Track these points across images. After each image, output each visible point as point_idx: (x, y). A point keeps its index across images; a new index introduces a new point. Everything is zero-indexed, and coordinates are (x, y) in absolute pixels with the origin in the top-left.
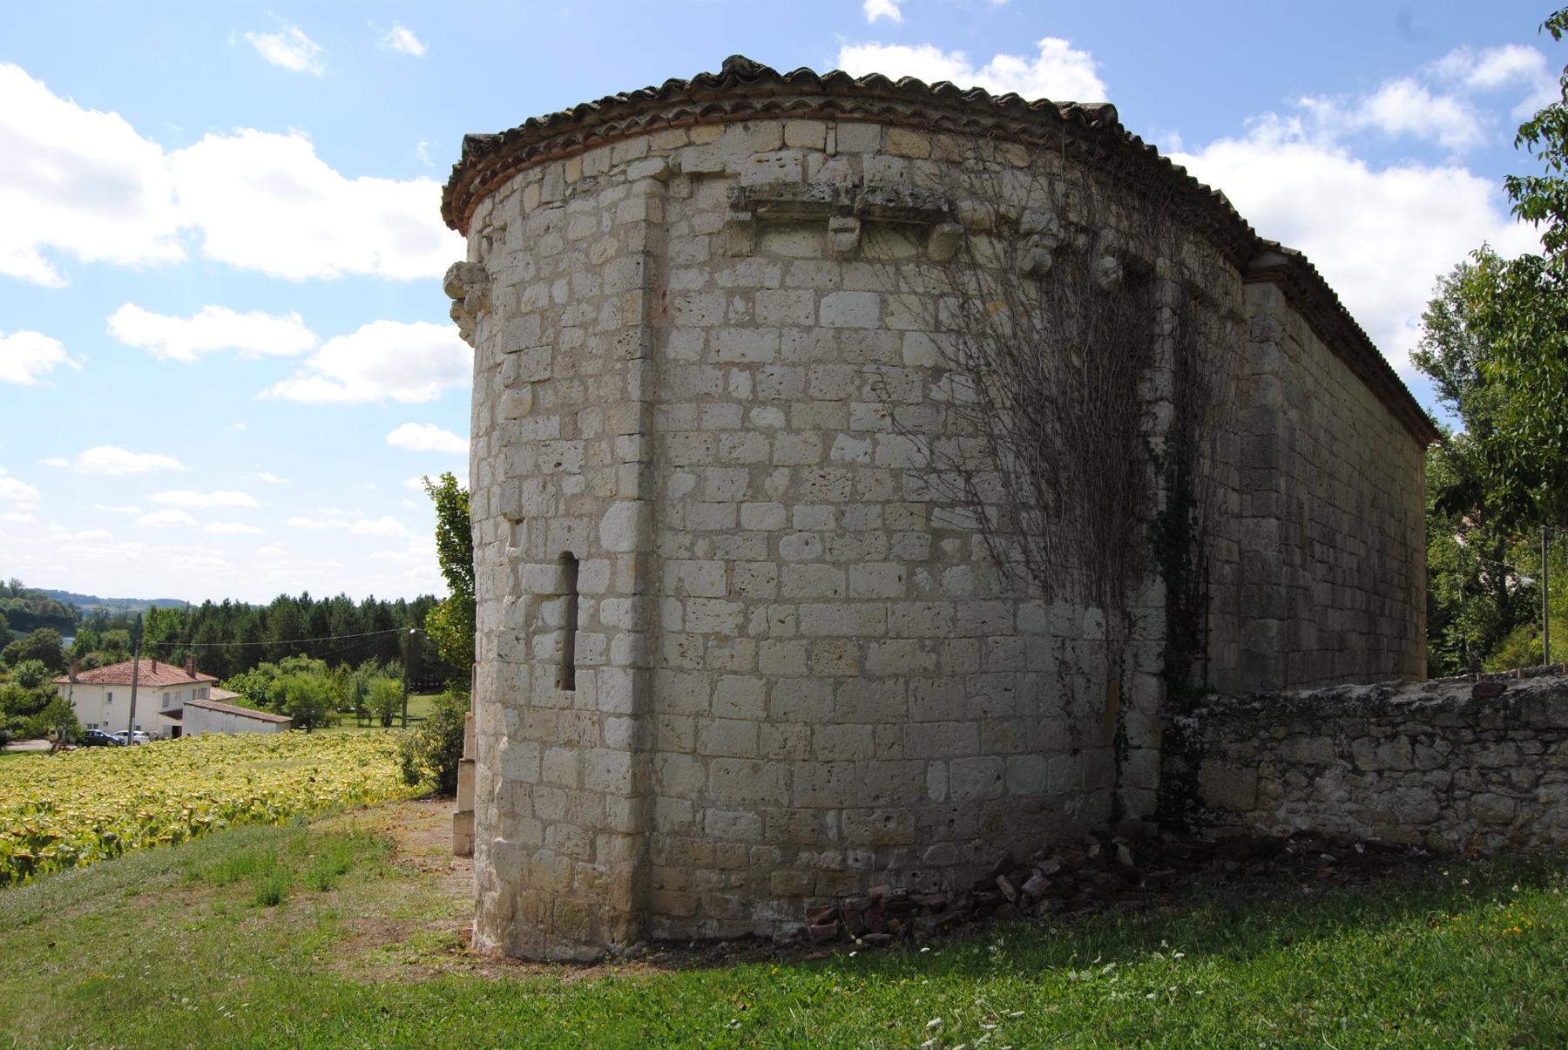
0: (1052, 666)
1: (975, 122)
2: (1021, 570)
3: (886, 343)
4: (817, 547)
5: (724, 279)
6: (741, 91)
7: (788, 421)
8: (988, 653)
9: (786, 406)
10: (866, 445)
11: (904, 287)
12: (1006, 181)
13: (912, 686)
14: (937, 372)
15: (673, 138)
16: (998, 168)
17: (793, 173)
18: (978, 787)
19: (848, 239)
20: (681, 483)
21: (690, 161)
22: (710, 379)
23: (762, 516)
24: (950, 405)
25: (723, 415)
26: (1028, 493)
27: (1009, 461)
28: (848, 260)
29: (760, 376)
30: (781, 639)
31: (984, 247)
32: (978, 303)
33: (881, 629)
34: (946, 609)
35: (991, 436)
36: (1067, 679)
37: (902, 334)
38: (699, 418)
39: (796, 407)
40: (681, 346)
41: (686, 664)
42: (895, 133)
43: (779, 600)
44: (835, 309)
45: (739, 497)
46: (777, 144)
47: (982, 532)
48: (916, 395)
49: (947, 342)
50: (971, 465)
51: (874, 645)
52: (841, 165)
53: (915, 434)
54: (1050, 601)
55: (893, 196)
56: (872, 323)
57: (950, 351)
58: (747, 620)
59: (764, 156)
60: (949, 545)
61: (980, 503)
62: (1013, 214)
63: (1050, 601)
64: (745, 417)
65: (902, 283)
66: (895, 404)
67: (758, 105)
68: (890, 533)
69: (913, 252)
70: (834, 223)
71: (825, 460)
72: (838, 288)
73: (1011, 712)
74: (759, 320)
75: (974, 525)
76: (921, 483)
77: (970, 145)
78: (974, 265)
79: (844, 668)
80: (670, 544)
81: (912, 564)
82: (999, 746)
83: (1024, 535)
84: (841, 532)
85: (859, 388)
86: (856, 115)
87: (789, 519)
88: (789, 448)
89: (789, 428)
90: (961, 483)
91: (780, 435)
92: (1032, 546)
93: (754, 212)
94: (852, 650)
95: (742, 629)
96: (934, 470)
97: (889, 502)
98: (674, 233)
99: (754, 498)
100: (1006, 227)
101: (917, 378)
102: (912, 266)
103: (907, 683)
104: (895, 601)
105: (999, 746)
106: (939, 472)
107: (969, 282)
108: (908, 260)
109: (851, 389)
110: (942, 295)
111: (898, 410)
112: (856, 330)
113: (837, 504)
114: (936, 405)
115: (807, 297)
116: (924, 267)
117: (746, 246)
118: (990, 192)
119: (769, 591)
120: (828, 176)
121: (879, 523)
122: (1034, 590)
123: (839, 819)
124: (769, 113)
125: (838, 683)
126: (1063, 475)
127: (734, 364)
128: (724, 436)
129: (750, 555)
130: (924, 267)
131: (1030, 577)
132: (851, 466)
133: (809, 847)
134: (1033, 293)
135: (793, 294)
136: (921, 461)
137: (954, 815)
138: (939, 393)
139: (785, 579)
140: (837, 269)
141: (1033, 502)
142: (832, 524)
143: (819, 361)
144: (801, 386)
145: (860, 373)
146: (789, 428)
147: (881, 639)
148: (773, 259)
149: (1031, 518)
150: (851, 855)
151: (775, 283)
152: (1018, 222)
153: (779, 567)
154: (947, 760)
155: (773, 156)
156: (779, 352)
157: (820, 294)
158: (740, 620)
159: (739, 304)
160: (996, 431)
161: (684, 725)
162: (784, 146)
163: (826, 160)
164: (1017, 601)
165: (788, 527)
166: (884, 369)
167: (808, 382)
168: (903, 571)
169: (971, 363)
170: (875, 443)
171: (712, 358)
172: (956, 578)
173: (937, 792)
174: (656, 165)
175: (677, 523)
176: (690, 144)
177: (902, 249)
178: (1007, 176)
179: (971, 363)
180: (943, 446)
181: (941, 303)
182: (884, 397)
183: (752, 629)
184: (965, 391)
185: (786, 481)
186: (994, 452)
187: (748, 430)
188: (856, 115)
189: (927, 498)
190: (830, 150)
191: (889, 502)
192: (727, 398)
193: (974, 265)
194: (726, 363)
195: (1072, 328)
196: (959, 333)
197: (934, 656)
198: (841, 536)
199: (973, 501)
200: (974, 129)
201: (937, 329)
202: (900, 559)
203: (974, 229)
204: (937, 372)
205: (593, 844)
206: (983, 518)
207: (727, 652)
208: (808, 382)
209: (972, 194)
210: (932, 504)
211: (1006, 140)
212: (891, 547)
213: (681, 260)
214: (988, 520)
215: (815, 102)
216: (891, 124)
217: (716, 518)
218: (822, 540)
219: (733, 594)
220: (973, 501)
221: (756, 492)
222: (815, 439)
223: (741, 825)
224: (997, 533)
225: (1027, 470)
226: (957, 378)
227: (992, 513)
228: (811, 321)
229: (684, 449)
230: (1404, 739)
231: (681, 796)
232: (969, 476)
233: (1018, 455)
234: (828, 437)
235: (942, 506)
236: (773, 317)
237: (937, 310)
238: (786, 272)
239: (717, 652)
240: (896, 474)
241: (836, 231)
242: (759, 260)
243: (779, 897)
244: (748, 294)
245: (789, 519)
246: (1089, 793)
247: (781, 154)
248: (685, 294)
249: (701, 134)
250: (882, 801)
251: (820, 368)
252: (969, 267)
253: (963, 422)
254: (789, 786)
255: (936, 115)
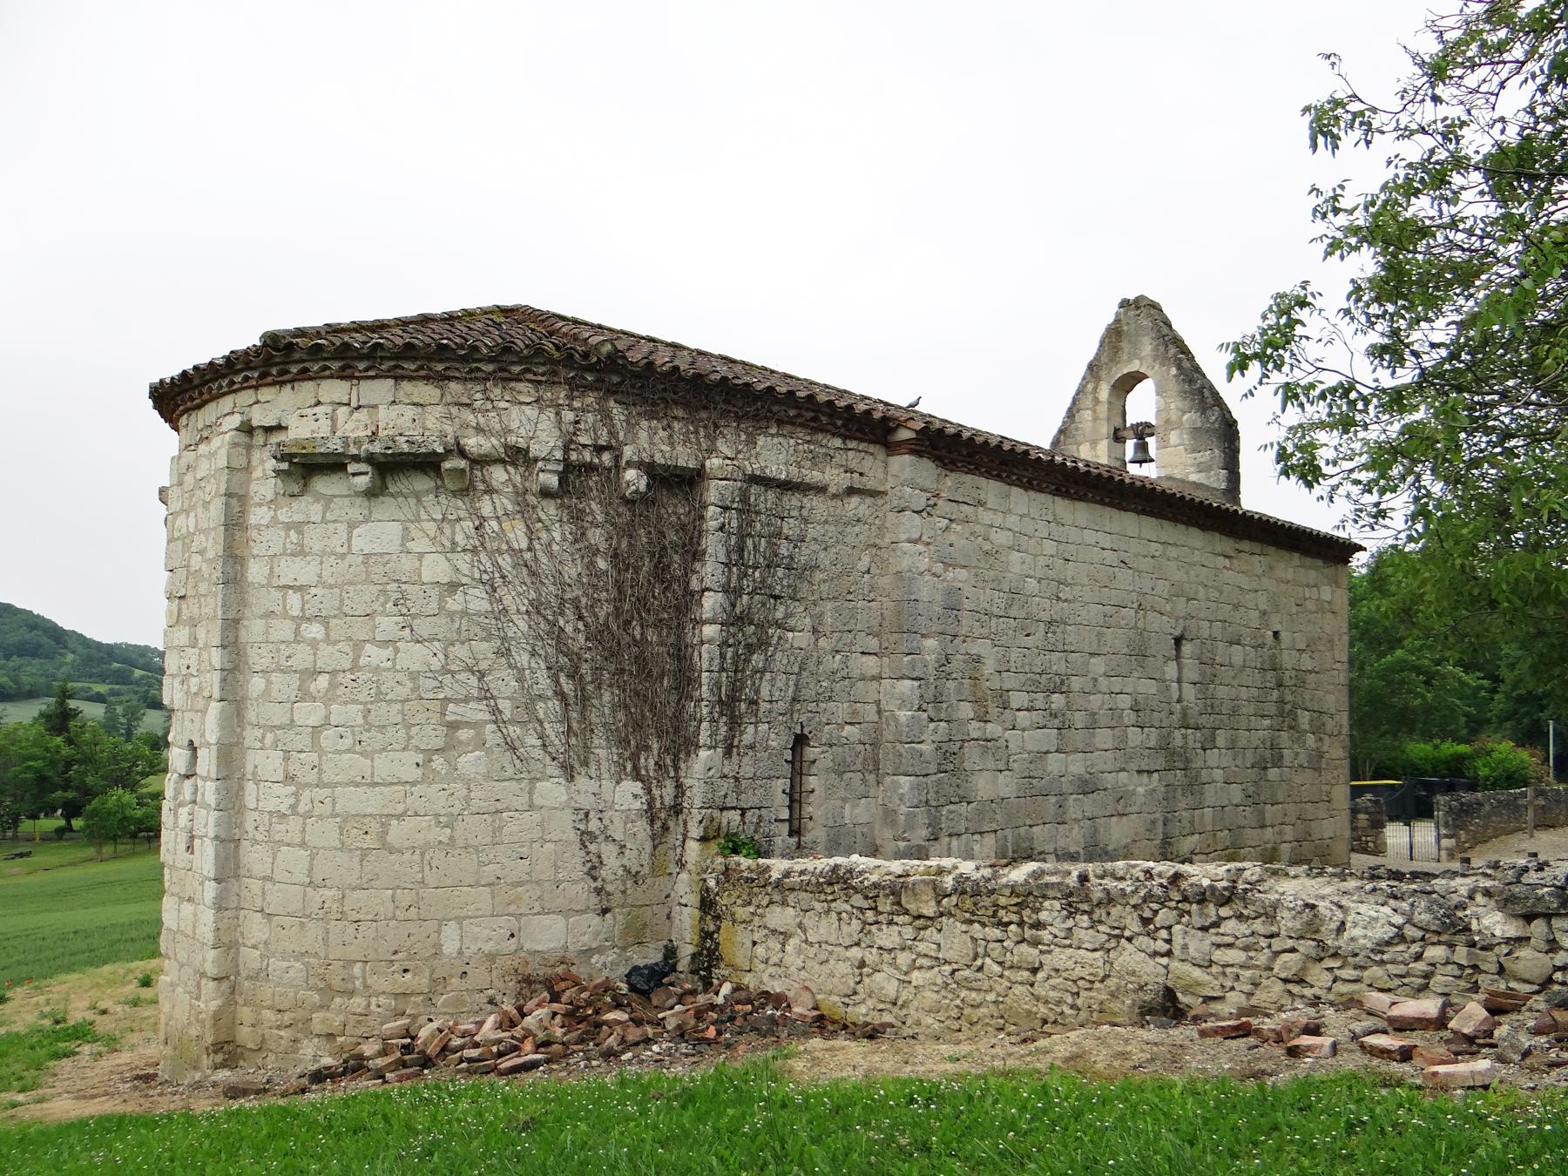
0: (573, 836)
1: (478, 369)
2: (538, 753)
3: (408, 564)
4: (348, 742)
5: (283, 515)
6: (282, 358)
7: (327, 635)
8: (501, 828)
9: (325, 621)
10: (389, 652)
11: (424, 516)
12: (514, 416)
13: (427, 857)
14: (453, 586)
15: (246, 397)
16: (507, 405)
17: (324, 428)
18: (491, 943)
19: (363, 482)
20: (256, 684)
21: (260, 418)
22: (272, 600)
23: (309, 714)
24: (465, 613)
25: (283, 630)
26: (544, 683)
27: (523, 659)
28: (375, 495)
29: (307, 597)
30: (321, 817)
31: (498, 475)
32: (494, 524)
33: (400, 808)
34: (459, 788)
35: (504, 639)
36: (592, 847)
37: (421, 555)
38: (267, 632)
39: (333, 622)
40: (256, 572)
41: (260, 837)
42: (406, 386)
43: (320, 784)
44: (364, 539)
45: (293, 698)
46: (313, 401)
47: (495, 722)
48: (433, 607)
49: (463, 562)
50: (484, 665)
51: (394, 822)
52: (362, 415)
53: (430, 641)
54: (571, 779)
55: (390, 444)
56: (394, 547)
57: (465, 568)
58: (298, 801)
59: (304, 412)
60: (464, 734)
61: (492, 697)
62: (522, 443)
63: (571, 779)
64: (297, 632)
65: (422, 513)
66: (414, 617)
67: (294, 369)
68: (409, 727)
69: (432, 484)
70: (351, 468)
71: (355, 667)
72: (367, 520)
73: (526, 877)
74: (307, 550)
75: (487, 717)
76: (437, 684)
77: (478, 388)
78: (490, 491)
79: (369, 841)
80: (251, 735)
81: (429, 753)
82: (512, 908)
83: (541, 723)
84: (368, 726)
85: (383, 605)
86: (371, 373)
87: (327, 717)
88: (329, 657)
89: (328, 640)
90: (474, 681)
91: (322, 646)
92: (549, 731)
93: (291, 462)
94: (375, 827)
95: (293, 807)
96: (449, 672)
97: (407, 700)
98: (254, 475)
99: (302, 700)
100: (517, 456)
101: (434, 593)
102: (431, 496)
103: (423, 854)
104: (413, 784)
105: (512, 908)
106: (453, 673)
107: (486, 507)
108: (428, 491)
109: (376, 606)
110: (459, 519)
111: (417, 621)
112: (381, 555)
113: (365, 704)
114: (451, 615)
115: (342, 528)
116: (442, 498)
117: (296, 489)
118: (498, 427)
119: (312, 777)
120: (354, 427)
121: (399, 719)
122: (553, 769)
123: (364, 971)
124: (304, 375)
125: (365, 853)
126: (585, 668)
127: (290, 587)
128: (283, 647)
129: (300, 747)
130: (442, 498)
131: (548, 759)
132: (377, 670)
133: (342, 993)
134: (552, 511)
135: (331, 527)
136: (436, 664)
137: (466, 969)
138: (455, 603)
139: (324, 767)
140: (366, 503)
141: (550, 693)
142: (360, 721)
143: (351, 583)
144: (337, 603)
145: (384, 592)
146: (328, 640)
147: (400, 817)
148: (319, 497)
149: (549, 709)
150: (374, 1000)
151: (318, 518)
152: (527, 451)
153: (320, 757)
154: (460, 920)
155: (310, 412)
156: (320, 576)
157: (352, 526)
158: (293, 800)
159: (293, 535)
160: (510, 634)
161: (255, 886)
162: (319, 403)
163: (351, 413)
164: (534, 780)
165: (326, 723)
166: (404, 587)
167: (342, 601)
168: (420, 758)
169: (485, 577)
170: (397, 651)
171: (275, 582)
172: (470, 762)
173: (450, 946)
174: (236, 420)
175: (254, 720)
176: (257, 402)
177: (422, 483)
178: (515, 411)
179: (485, 577)
180: (460, 651)
181: (458, 527)
182: (404, 611)
183: (301, 809)
184: (478, 600)
185: (326, 684)
186: (508, 653)
187: (299, 642)
188: (371, 373)
189: (441, 696)
190: (354, 404)
191: (407, 700)
192: (286, 615)
193: (490, 491)
194: (284, 587)
195: (596, 536)
196: (474, 551)
197: (448, 831)
198: (368, 731)
199: (486, 696)
200: (479, 374)
201: (453, 551)
202: (418, 749)
203: (481, 462)
204: (453, 586)
205: (199, 986)
206: (496, 711)
207: (282, 827)
208: (342, 601)
209: (479, 430)
210: (447, 700)
211: (511, 380)
212: (410, 738)
213: (256, 499)
214: (501, 712)
215: (335, 365)
216: (403, 378)
217: (278, 715)
218: (353, 733)
219: (289, 778)
220: (486, 696)
221: (304, 695)
222: (347, 649)
223: (292, 974)
224: (513, 722)
225: (543, 666)
226: (471, 591)
227: (505, 706)
228: (344, 550)
229: (258, 657)
230: (834, 915)
231: (254, 947)
232: (482, 675)
233: (533, 654)
234: (358, 646)
235: (457, 701)
236: (317, 547)
237: (454, 533)
238: (326, 508)
239: (279, 827)
240: (414, 676)
241: (354, 475)
242: (308, 498)
243: (319, 1036)
244: (298, 527)
245: (327, 717)
246: (624, 949)
247: (316, 410)
248: (258, 528)
249: (266, 394)
250: (400, 955)
251: (351, 589)
252: (486, 492)
253: (477, 629)
254: (325, 940)
255: (440, 367)
